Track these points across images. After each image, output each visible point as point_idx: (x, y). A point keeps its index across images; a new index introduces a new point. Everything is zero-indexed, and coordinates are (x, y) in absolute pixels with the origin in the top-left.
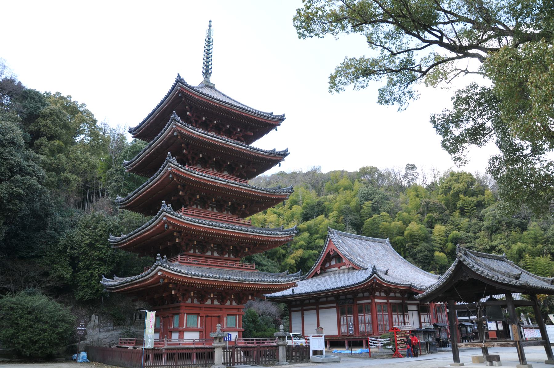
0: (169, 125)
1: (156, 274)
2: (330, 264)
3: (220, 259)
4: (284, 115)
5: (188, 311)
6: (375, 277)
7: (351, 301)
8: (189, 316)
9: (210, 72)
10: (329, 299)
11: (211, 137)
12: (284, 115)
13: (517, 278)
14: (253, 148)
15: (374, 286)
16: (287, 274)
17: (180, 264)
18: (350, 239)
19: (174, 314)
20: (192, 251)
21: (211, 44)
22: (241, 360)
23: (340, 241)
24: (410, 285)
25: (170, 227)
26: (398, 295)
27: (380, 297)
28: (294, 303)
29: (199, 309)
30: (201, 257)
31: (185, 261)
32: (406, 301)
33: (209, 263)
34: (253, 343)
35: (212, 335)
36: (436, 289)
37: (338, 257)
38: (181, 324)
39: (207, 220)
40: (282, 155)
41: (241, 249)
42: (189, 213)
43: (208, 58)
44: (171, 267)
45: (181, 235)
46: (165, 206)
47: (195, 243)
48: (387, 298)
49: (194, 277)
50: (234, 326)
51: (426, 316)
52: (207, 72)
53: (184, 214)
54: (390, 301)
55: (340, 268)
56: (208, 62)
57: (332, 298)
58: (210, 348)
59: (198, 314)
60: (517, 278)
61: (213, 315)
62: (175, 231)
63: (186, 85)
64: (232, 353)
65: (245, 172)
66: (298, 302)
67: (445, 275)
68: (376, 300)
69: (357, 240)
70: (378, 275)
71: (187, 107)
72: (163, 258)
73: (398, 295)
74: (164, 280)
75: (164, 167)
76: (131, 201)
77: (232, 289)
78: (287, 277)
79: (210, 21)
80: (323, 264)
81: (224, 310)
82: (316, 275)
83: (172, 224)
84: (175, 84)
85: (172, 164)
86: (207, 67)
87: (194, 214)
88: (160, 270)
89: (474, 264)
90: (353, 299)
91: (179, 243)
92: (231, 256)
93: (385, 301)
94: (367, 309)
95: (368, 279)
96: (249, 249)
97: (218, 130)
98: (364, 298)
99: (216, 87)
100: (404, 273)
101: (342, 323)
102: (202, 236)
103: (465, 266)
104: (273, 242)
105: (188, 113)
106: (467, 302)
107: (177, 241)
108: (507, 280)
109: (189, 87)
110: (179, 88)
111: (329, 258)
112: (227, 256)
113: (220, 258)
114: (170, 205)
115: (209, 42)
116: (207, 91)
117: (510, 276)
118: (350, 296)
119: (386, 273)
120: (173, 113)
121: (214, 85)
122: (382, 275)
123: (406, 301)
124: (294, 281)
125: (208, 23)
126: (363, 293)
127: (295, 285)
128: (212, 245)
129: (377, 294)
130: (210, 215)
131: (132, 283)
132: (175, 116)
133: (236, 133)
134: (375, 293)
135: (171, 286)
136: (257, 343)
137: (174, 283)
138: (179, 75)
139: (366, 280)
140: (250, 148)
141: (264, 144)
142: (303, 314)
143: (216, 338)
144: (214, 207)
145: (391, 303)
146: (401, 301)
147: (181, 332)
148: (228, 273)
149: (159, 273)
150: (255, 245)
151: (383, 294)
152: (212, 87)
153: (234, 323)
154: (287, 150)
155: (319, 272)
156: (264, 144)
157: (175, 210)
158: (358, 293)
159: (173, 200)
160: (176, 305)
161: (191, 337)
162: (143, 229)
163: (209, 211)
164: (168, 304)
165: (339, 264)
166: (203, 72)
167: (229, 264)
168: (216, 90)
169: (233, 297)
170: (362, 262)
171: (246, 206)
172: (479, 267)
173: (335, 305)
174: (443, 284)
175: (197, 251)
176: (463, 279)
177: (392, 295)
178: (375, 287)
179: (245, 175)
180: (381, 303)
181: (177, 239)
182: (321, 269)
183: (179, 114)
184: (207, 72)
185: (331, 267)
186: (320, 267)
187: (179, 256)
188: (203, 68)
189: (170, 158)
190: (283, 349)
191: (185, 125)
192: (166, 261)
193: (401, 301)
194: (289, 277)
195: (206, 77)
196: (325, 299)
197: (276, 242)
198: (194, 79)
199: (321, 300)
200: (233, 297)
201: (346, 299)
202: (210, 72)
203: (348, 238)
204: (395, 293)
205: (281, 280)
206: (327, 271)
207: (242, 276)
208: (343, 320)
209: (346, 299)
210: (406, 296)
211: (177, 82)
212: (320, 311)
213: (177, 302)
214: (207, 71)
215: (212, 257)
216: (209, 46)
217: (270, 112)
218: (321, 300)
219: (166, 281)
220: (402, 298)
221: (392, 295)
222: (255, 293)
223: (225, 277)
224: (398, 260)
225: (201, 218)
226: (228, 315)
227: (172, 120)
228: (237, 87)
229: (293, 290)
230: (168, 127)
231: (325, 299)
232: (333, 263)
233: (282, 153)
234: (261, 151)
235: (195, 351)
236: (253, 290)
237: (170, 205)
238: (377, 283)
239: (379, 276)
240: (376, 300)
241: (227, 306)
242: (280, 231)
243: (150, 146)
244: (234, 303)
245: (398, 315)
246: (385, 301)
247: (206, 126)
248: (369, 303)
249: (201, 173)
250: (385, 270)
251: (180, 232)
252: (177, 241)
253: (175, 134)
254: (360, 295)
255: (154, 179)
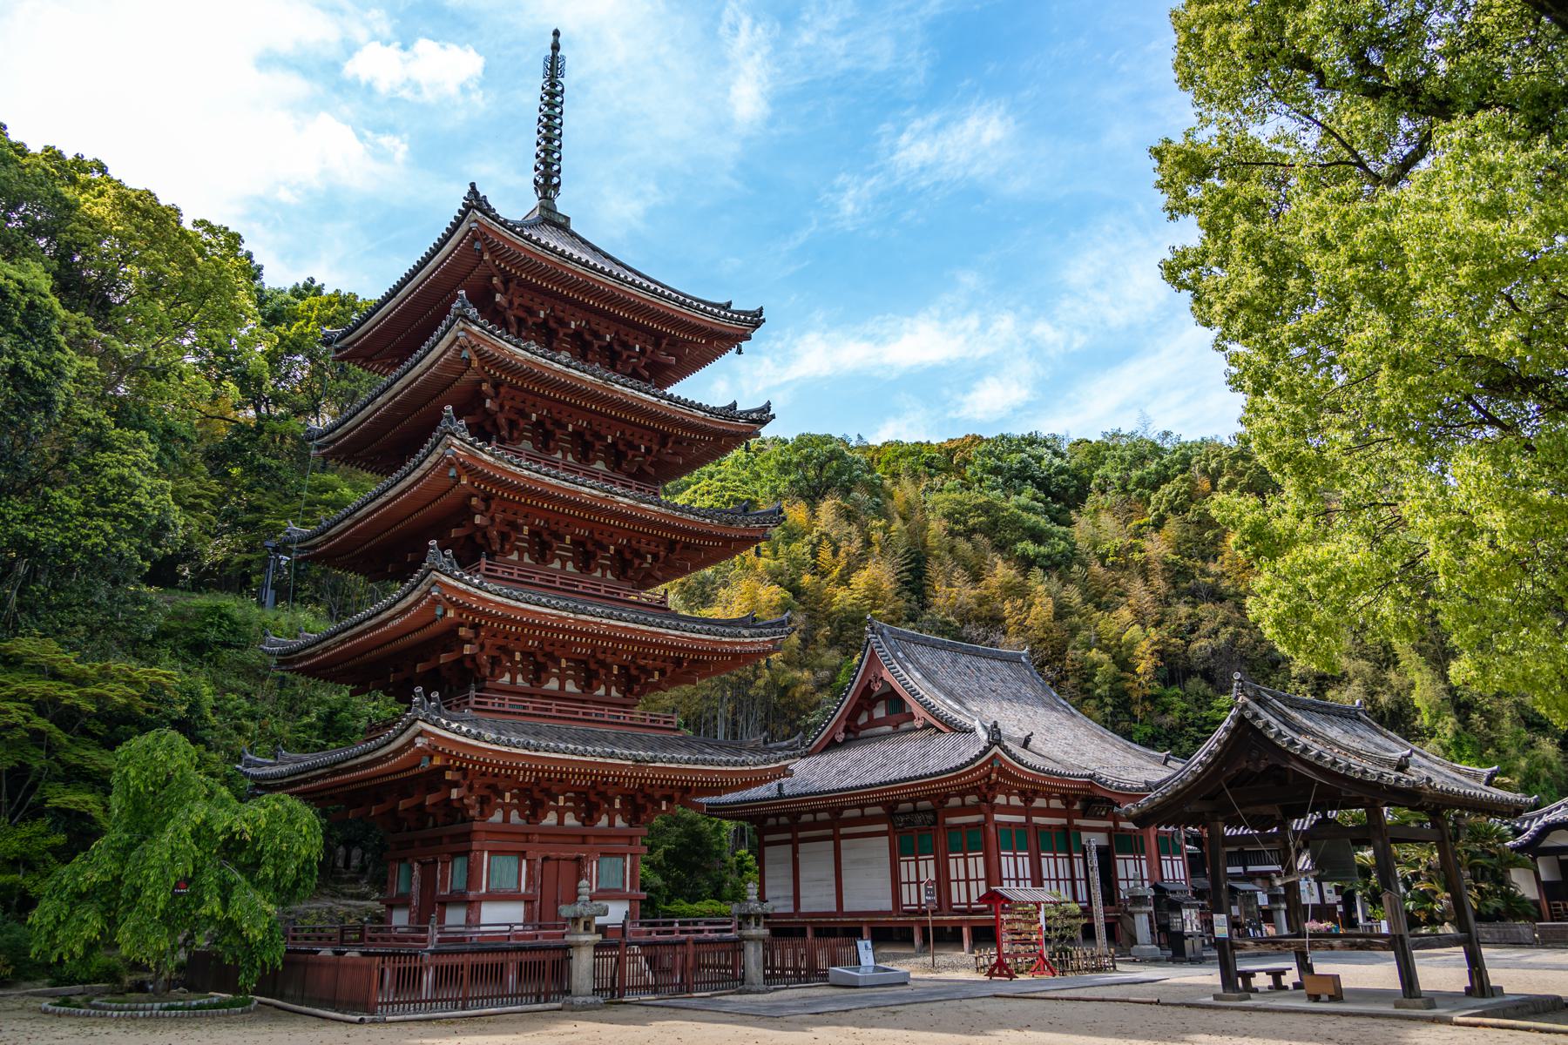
0: (448, 328)
1: (411, 743)
2: (871, 717)
3: (584, 701)
4: (761, 310)
5: (493, 844)
6: (995, 755)
7: (930, 817)
8: (495, 859)
9: (555, 180)
10: (868, 811)
11: (560, 366)
12: (761, 310)
13: (1402, 766)
14: (678, 401)
15: (994, 776)
16: (765, 742)
17: (476, 714)
18: (927, 649)
19: (455, 855)
20: (507, 678)
21: (559, 99)
22: (641, 981)
23: (900, 654)
24: (1090, 776)
25: (451, 614)
26: (1056, 804)
27: (1008, 809)
28: (771, 821)
29: (523, 838)
30: (531, 695)
31: (489, 707)
32: (1076, 822)
33: (554, 713)
34: (672, 932)
35: (566, 911)
36: (1178, 792)
37: (894, 700)
38: (472, 879)
39: (551, 593)
40: (753, 421)
41: (631, 672)
42: (499, 574)
43: (549, 140)
44: (454, 725)
45: (477, 635)
46: (437, 555)
47: (518, 657)
48: (1028, 811)
49: (514, 750)
50: (620, 886)
51: (1131, 863)
52: (548, 183)
53: (486, 576)
54: (1035, 819)
55: (897, 726)
56: (549, 152)
57: (879, 810)
58: (556, 948)
59: (522, 854)
60: (1402, 766)
61: (564, 855)
62: (462, 625)
63: (496, 218)
64: (618, 961)
65: (652, 464)
66: (783, 820)
67: (1201, 755)
68: (997, 817)
69: (944, 654)
70: (1005, 749)
71: (495, 280)
72: (430, 700)
73: (1056, 804)
74: (431, 758)
75: (435, 446)
76: (330, 539)
77: (561, 780)
78: (763, 751)
79: (556, 33)
80: (852, 716)
81: (592, 840)
82: (831, 746)
83: (455, 605)
84: (464, 214)
85: (457, 442)
86: (548, 165)
87: (515, 577)
88: (421, 733)
89: (1283, 728)
90: (934, 812)
91: (473, 657)
92: (614, 693)
93: (1022, 819)
94: (978, 840)
95: (977, 757)
96: (663, 673)
97: (582, 348)
98: (964, 810)
99: (573, 227)
100: (1067, 744)
101: (904, 879)
102: (534, 638)
103: (1258, 732)
104: (727, 654)
105: (498, 297)
106: (1256, 824)
107: (466, 652)
108: (1373, 770)
109: (504, 223)
110: (474, 225)
111: (867, 699)
112: (601, 692)
113: (583, 697)
114: (449, 552)
115: (553, 95)
116: (549, 238)
117: (1383, 762)
118: (926, 804)
119: (1026, 744)
120: (457, 296)
121: (568, 219)
122: (1016, 749)
123: (1076, 822)
124: (783, 763)
125: (551, 39)
126: (962, 794)
127: (786, 772)
128: (564, 663)
129: (1001, 799)
130: (558, 580)
131: (334, 768)
132: (464, 306)
133: (630, 357)
134: (994, 797)
135: (449, 776)
136: (682, 932)
137: (459, 769)
138: (473, 185)
139: (973, 761)
140: (670, 398)
141: (710, 387)
142: (795, 852)
143: (576, 920)
144: (569, 559)
145: (1037, 826)
146: (1065, 821)
147: (472, 905)
148: (606, 739)
149: (420, 742)
150: (678, 662)
151: (1015, 801)
152: (561, 225)
153: (620, 878)
154: (768, 407)
155: (840, 737)
156: (710, 387)
157: (462, 566)
158: (948, 796)
159: (457, 539)
160: (458, 828)
161: (502, 916)
162: (370, 618)
163: (596, 579)
164: (435, 825)
165: (896, 717)
166: (536, 182)
167: (607, 713)
168: (573, 235)
169: (617, 806)
170: (959, 713)
171: (655, 557)
172: (1295, 736)
173: (884, 827)
174: (1196, 780)
175: (613, 690)
176: (1251, 768)
177: (1040, 803)
178: (997, 782)
179: (652, 471)
180: (1010, 824)
181: (467, 647)
182: (847, 730)
183: (473, 299)
184: (548, 183)
185: (873, 722)
186: (844, 724)
187: (473, 693)
188: (536, 169)
189: (451, 422)
190: (757, 950)
191: (491, 332)
192: (438, 708)
193: (1065, 821)
194: (771, 751)
195: (545, 197)
196: (856, 812)
197: (736, 656)
198: (514, 200)
199: (847, 813)
200: (617, 806)
201: (916, 811)
202: (555, 180)
203: (920, 648)
204: (1048, 797)
205: (753, 763)
206: (861, 734)
207: (645, 749)
208: (907, 869)
209: (916, 811)
210: (1077, 807)
211: (468, 208)
212: (802, 846)
213: (464, 820)
214: (548, 176)
215: (561, 694)
216: (552, 106)
217: (722, 301)
218: (847, 813)
219: (437, 761)
220: (1067, 813)
221: (1040, 803)
222: (677, 795)
223: (599, 749)
224: (1054, 709)
225: (533, 589)
226: (604, 854)
227: (457, 316)
228: (618, 218)
229: (780, 786)
230: (444, 334)
231: (857, 812)
232: (880, 713)
233: (755, 415)
234: (699, 407)
235: (512, 956)
236: (672, 787)
237: (449, 552)
238: (1002, 772)
239: (1008, 752)
240: (997, 817)
241: (601, 829)
242: (747, 627)
243: (389, 386)
244: (619, 822)
245: (1055, 858)
246: (1022, 819)
247: (548, 336)
248: (977, 825)
249: (535, 466)
250: (1022, 735)
251: (475, 627)
252: (466, 652)
253: (465, 354)
254: (955, 802)
255: (403, 478)
